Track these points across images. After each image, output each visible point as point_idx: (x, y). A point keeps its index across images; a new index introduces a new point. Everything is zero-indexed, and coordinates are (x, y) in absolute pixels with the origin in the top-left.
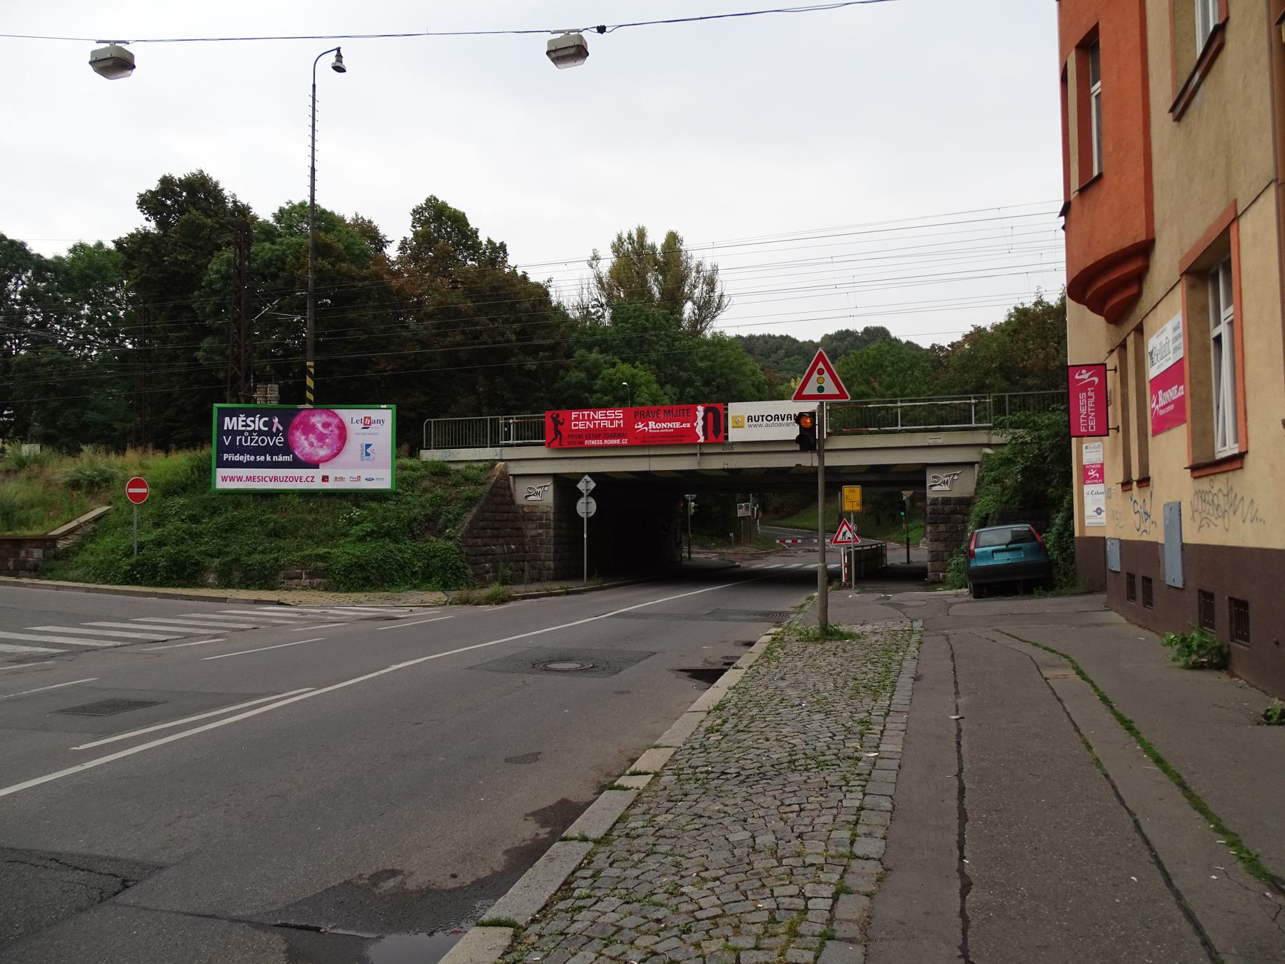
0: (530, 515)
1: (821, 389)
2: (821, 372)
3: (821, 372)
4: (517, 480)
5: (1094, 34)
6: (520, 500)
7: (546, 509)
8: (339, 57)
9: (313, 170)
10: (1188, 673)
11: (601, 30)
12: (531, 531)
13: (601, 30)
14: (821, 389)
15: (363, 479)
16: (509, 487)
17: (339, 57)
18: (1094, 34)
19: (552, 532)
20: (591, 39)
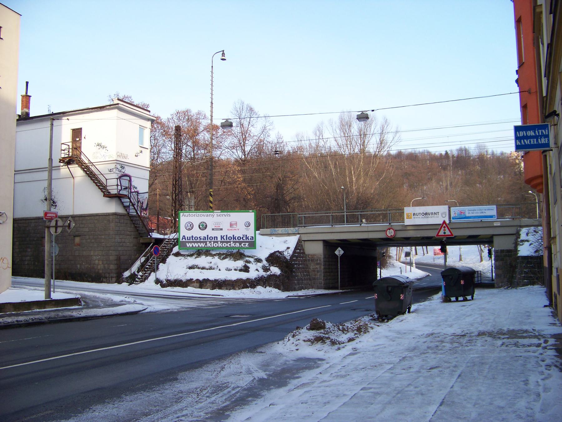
0: (313, 259)
1: (445, 233)
2: (444, 227)
3: (444, 227)
4: (306, 242)
5: (520, 17)
6: (307, 252)
7: (319, 256)
8: (223, 54)
9: (212, 103)
10: (400, 323)
11: (373, 111)
12: (312, 266)
13: (373, 111)
14: (445, 233)
15: (196, 227)
16: (302, 246)
17: (223, 54)
18: (520, 17)
19: (322, 267)
20: (370, 113)
